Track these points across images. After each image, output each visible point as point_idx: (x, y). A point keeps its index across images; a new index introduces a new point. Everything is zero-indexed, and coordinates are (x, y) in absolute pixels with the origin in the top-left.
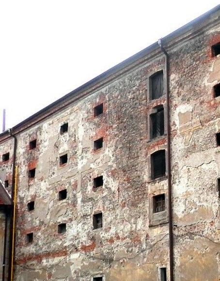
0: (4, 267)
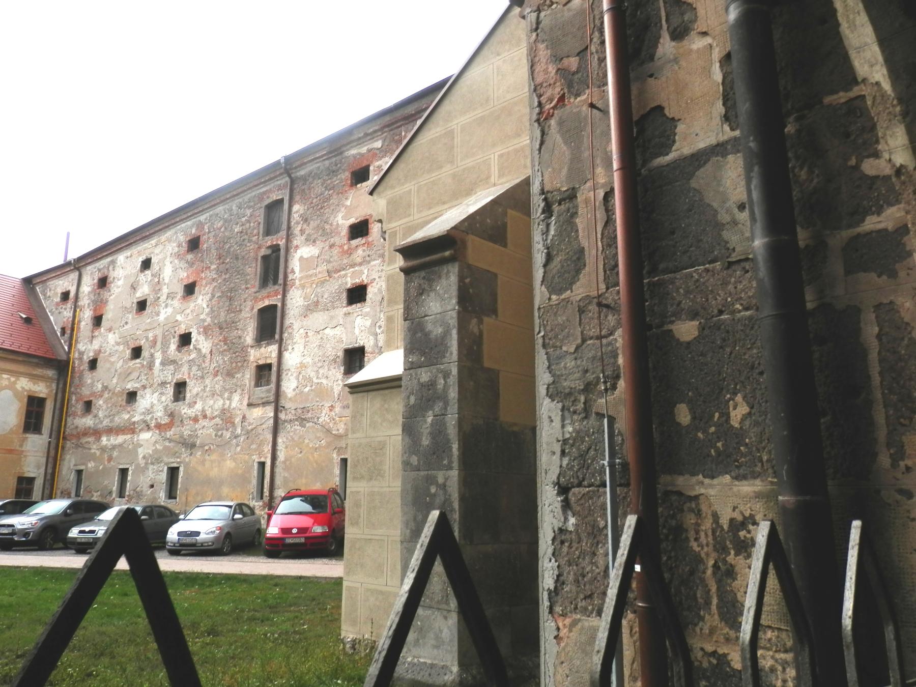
0: (50, 442)
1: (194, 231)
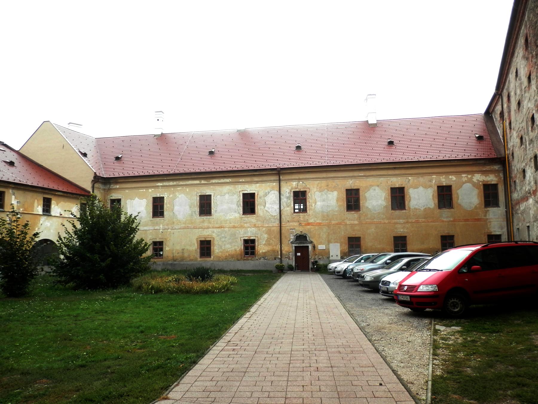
0: (506, 212)
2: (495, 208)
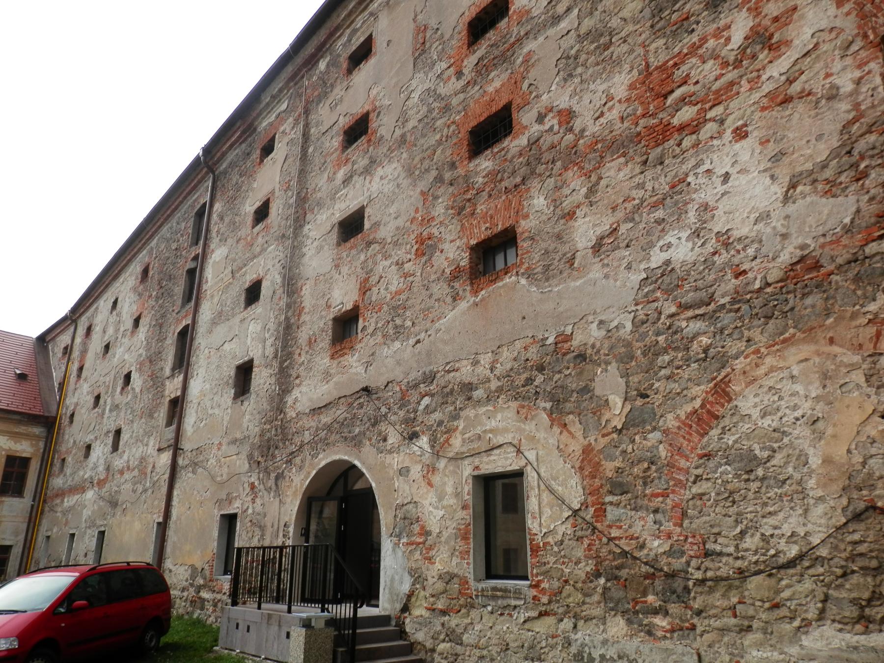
0: (32, 506)
1: (147, 259)
2: (15, 499)
